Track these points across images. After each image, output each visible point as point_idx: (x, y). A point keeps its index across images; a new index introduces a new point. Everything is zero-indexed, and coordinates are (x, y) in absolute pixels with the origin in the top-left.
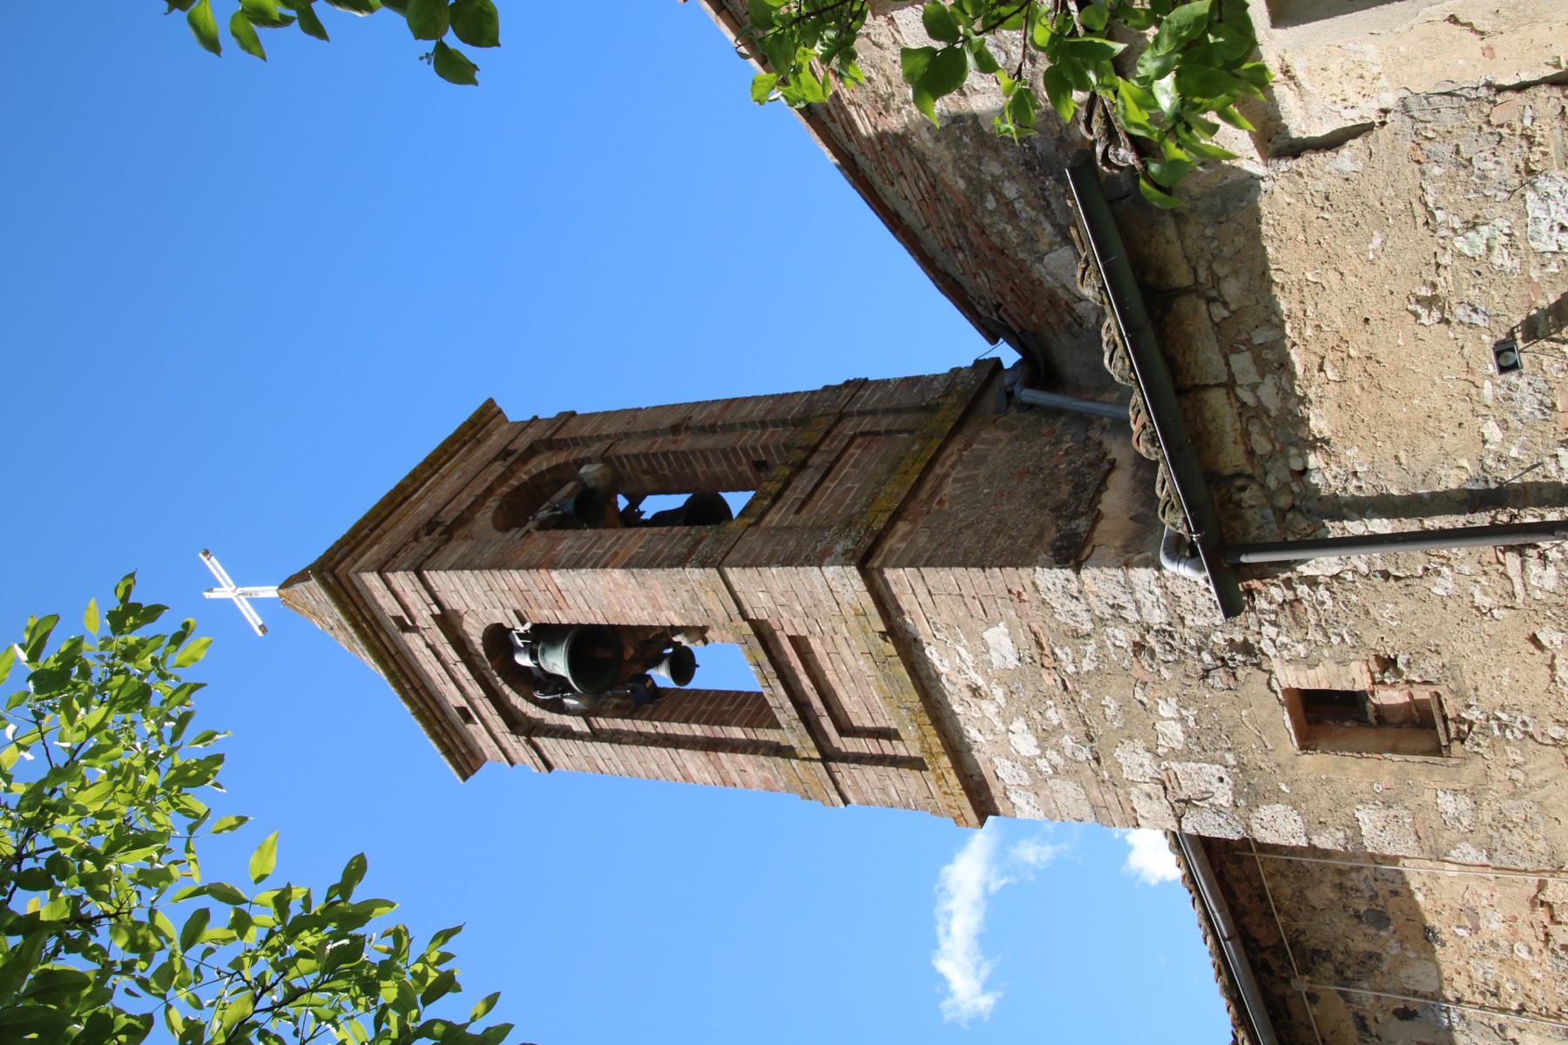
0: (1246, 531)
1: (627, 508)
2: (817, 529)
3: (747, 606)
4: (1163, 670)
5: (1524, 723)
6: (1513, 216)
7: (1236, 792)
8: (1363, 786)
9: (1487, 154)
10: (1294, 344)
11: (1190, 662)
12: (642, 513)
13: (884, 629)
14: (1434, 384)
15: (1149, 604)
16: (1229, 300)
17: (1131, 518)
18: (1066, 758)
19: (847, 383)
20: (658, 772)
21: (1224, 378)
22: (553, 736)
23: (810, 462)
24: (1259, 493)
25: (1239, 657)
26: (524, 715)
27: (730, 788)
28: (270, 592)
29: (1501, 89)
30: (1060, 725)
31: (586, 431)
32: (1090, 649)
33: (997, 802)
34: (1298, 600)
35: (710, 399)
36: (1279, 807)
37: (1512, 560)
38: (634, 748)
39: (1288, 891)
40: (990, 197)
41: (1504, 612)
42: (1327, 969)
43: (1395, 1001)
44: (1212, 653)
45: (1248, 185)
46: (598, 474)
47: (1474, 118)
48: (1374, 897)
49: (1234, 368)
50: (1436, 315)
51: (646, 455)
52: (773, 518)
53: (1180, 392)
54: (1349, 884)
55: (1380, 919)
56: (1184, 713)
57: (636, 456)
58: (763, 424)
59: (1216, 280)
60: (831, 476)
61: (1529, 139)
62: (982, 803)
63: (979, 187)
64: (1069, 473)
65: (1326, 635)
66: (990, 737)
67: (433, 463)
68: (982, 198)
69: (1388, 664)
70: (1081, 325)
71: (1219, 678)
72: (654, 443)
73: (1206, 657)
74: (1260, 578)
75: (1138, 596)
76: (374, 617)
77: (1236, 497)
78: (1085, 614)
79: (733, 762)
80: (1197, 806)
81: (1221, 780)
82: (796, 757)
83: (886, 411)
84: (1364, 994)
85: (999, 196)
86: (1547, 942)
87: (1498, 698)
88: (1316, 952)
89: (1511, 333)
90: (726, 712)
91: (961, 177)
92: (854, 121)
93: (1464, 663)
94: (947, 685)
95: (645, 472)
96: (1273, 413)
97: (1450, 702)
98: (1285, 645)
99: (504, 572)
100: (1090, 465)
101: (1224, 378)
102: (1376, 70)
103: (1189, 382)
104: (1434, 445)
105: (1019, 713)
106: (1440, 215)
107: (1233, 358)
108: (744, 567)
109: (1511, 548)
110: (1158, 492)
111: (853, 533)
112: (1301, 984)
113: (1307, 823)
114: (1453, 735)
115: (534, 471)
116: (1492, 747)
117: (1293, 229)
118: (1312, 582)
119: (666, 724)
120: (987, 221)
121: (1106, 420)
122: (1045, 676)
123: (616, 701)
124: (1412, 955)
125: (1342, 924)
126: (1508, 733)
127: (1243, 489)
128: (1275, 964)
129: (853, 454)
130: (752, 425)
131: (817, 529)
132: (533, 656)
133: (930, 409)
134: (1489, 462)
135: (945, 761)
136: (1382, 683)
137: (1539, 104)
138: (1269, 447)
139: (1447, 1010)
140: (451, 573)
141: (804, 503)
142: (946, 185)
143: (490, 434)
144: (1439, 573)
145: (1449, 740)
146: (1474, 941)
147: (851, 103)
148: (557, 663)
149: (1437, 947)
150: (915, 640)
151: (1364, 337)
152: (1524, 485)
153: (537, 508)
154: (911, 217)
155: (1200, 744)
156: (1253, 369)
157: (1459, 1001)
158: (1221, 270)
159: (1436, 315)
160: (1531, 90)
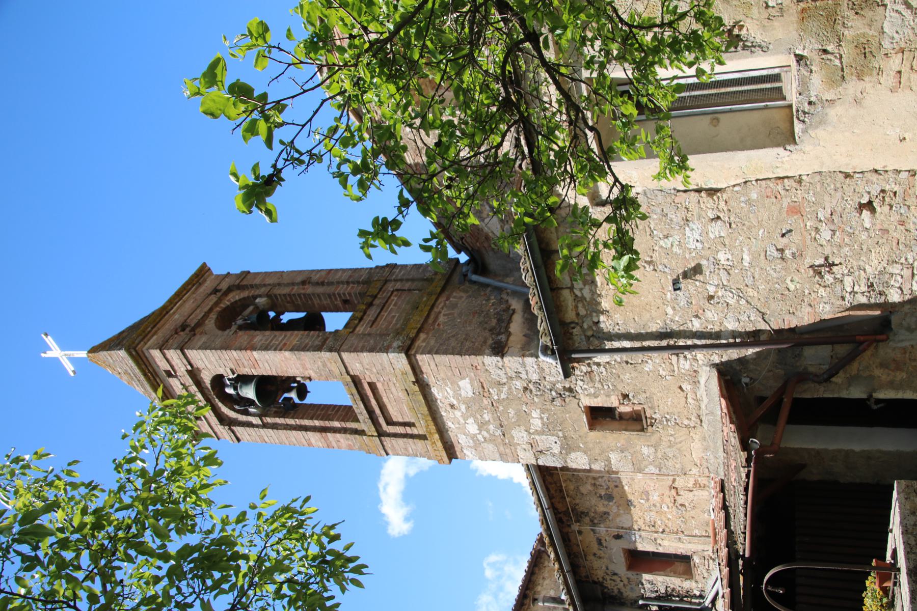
0: (574, 344)
1: (274, 317)
2: (383, 335)
3: (350, 369)
5: (675, 419)
6: (681, 235)
7: (562, 448)
8: (613, 444)
9: (673, 212)
11: (547, 395)
12: (281, 320)
13: (414, 380)
17: (524, 335)
18: (490, 434)
19: (387, 265)
20: (295, 442)
21: (569, 285)
22: (242, 426)
23: (374, 303)
25: (567, 393)
26: (227, 416)
27: (331, 449)
28: (83, 354)
29: (678, 191)
30: (489, 421)
31: (257, 281)
33: (458, 453)
34: (592, 371)
35: (320, 269)
36: (579, 453)
37: (674, 358)
38: (285, 431)
39: (572, 487)
41: (670, 377)
42: (587, 520)
43: (614, 532)
44: (556, 392)
46: (265, 303)
47: (669, 200)
48: (608, 488)
50: (652, 267)
51: (289, 295)
52: (360, 329)
53: (552, 290)
54: (598, 483)
55: (610, 498)
56: (543, 415)
57: (284, 295)
58: (348, 283)
60: (385, 308)
61: (687, 209)
62: (451, 454)
64: (495, 314)
65: (602, 385)
66: (457, 426)
67: (179, 295)
69: (626, 396)
71: (558, 402)
72: (293, 289)
73: (554, 393)
74: (578, 362)
75: (527, 368)
76: (154, 370)
77: (571, 331)
79: (334, 437)
82: (366, 435)
83: (407, 280)
84: (601, 529)
86: (675, 503)
88: (582, 513)
89: (678, 276)
90: (330, 415)
94: (440, 404)
95: (288, 302)
96: (588, 300)
98: (586, 389)
99: (228, 352)
100: (504, 311)
102: (636, 180)
103: (555, 286)
104: (648, 315)
105: (472, 415)
106: (655, 232)
108: (350, 352)
109: (674, 354)
110: (539, 327)
111: (401, 338)
112: (575, 527)
113: (590, 460)
115: (233, 300)
116: (663, 428)
118: (598, 364)
119: (301, 420)
121: (509, 291)
123: (274, 409)
124: (622, 512)
125: (594, 500)
127: (574, 328)
128: (565, 519)
129: (393, 300)
130: (342, 283)
131: (383, 335)
132: (235, 389)
133: (429, 280)
135: (437, 436)
136: (623, 404)
137: (691, 198)
138: (585, 313)
139: (635, 534)
140: (200, 351)
141: (374, 322)
143: (205, 281)
144: (647, 362)
146: (647, 505)
148: (249, 392)
149: (632, 508)
150: (427, 385)
153: (235, 320)
155: (548, 428)
157: (639, 530)
159: (652, 267)
160: (689, 193)
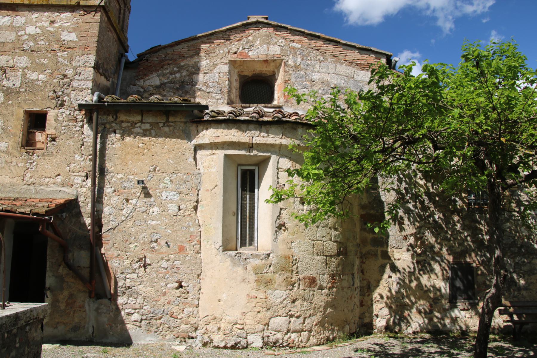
4: (57, 80)
5: (32, 168)
6: (172, 189)
10: (150, 139)
11: (59, 88)
14: (135, 166)
15: (80, 83)
16: (164, 128)
21: (144, 121)
24: (111, 121)
25: (59, 102)
29: (198, 191)
32: (66, 62)
40: (177, 70)
44: (61, 95)
45: (190, 139)
47: (194, 185)
49: (146, 124)
56: (41, 82)
59: (169, 126)
63: (181, 68)
68: (177, 68)
70: (137, 79)
73: (60, 93)
78: (78, 65)
80: (3, 75)
81: (14, 85)
85: (177, 72)
87: (40, 164)
91: (184, 65)
92: (205, 44)
93: (53, 158)
96: (133, 130)
97: (40, 152)
98: (62, 115)
101: (144, 121)
102: (209, 170)
107: (149, 125)
114: (28, 151)
117: (178, 146)
118: (82, 127)
120: (171, 66)
122: (57, 46)
126: (29, 164)
127: (113, 117)
134: (112, 174)
142: (183, 60)
144: (82, 157)
145: (26, 149)
147: (210, 46)
151: (149, 154)
152: (105, 180)
154: (177, 48)
156: (145, 128)
158: (171, 128)
159: (152, 170)
